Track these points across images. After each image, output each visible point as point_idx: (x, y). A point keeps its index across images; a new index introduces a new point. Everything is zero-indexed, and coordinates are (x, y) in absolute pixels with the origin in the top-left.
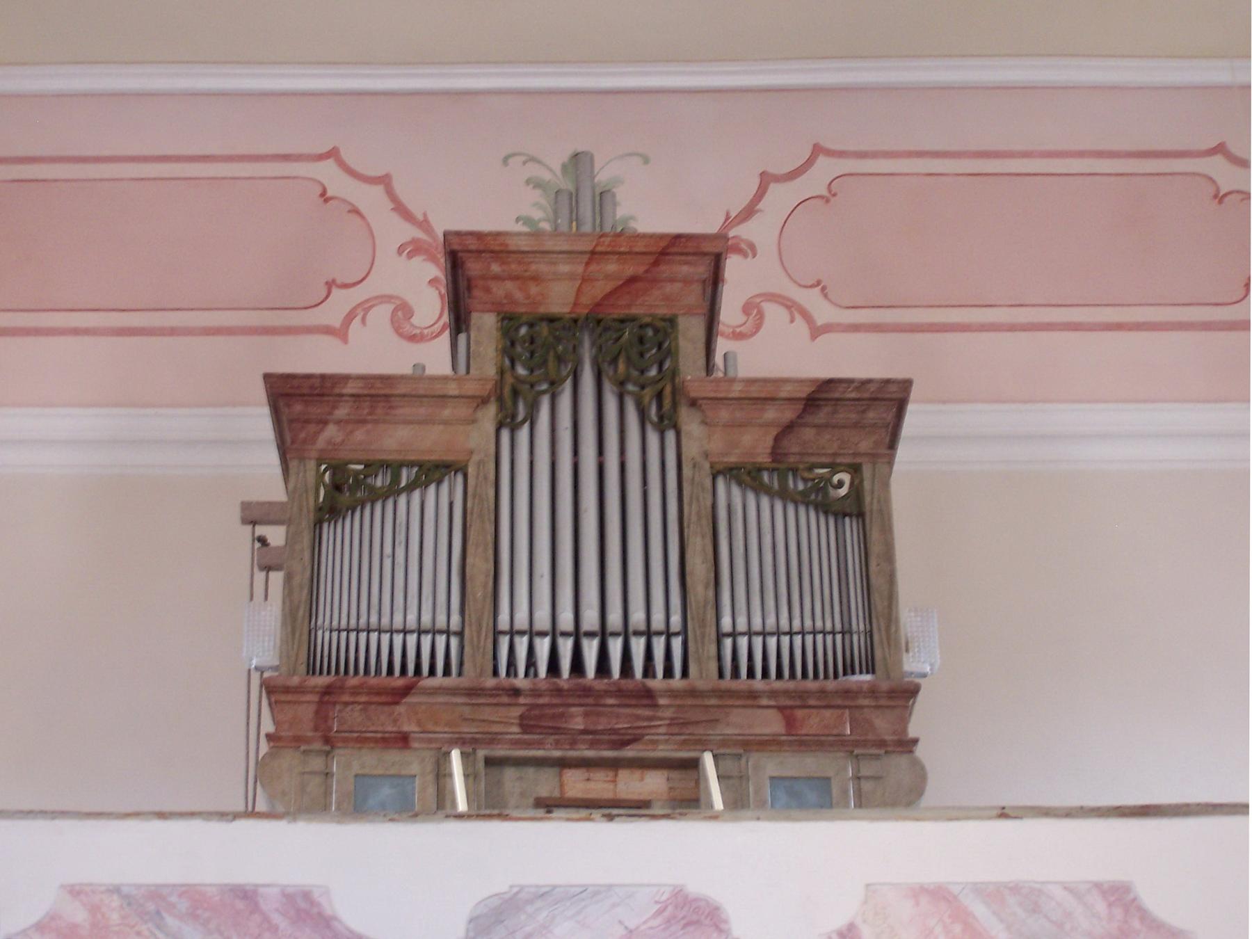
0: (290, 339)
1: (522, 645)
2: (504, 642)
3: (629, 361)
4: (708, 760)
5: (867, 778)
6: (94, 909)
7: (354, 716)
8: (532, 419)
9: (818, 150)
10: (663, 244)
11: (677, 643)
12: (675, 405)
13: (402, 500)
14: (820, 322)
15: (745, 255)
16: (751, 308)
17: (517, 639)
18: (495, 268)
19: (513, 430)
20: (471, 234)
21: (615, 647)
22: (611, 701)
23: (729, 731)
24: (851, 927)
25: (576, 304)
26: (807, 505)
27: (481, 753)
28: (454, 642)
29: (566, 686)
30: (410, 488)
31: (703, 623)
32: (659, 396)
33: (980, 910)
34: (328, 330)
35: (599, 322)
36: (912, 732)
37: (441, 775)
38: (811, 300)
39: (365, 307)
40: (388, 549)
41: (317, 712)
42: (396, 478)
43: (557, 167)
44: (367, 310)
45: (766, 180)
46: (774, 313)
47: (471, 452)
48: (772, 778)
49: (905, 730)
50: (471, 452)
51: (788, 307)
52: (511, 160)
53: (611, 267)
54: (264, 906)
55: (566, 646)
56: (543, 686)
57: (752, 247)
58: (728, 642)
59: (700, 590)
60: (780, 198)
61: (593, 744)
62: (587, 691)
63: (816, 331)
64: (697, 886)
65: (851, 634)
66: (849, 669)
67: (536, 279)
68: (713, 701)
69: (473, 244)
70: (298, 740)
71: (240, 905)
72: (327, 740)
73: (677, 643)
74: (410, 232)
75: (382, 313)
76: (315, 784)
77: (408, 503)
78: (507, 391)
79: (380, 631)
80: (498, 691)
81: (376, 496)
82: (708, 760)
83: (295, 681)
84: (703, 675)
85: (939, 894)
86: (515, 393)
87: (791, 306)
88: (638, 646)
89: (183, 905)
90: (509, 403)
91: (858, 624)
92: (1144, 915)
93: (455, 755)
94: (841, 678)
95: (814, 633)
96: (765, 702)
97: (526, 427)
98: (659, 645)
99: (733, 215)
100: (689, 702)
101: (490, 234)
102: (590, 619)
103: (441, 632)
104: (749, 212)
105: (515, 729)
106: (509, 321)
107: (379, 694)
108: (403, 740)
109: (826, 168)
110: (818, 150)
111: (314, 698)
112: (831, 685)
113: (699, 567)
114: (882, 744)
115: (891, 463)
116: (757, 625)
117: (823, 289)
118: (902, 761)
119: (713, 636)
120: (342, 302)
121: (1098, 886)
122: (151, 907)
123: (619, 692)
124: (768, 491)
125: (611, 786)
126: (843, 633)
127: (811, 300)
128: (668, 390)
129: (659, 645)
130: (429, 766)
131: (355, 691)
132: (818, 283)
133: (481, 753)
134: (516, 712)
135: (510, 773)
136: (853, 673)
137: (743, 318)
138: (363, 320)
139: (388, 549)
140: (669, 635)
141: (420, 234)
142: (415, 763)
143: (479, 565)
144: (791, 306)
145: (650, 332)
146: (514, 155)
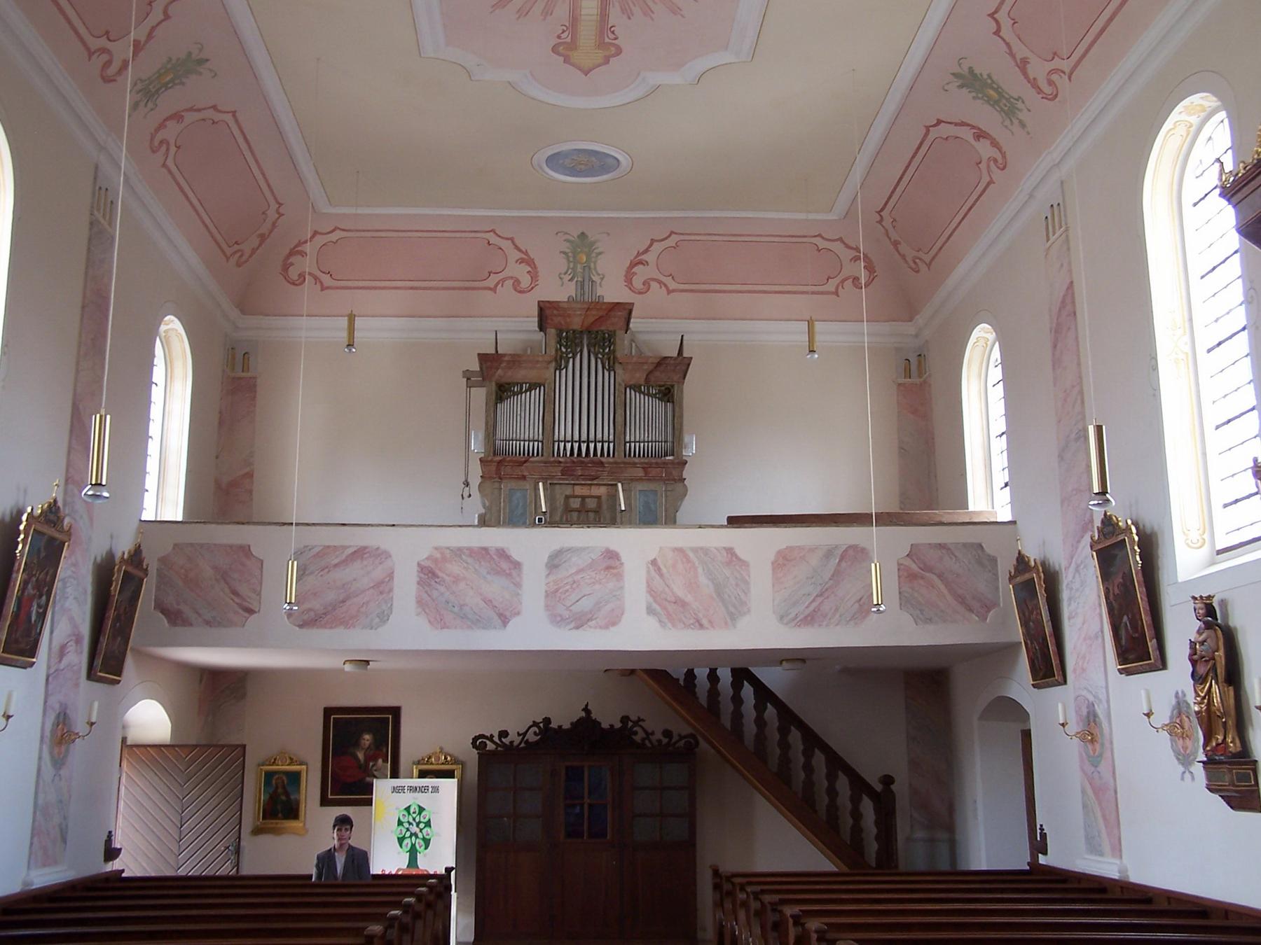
0: (475, 292)
1: (562, 445)
2: (556, 444)
3: (599, 345)
4: (620, 485)
5: (669, 491)
6: (442, 554)
7: (508, 470)
8: (566, 367)
9: (672, 233)
10: (612, 306)
11: (611, 445)
12: (614, 363)
13: (524, 395)
14: (671, 288)
15: (644, 265)
16: (646, 283)
17: (560, 443)
18: (555, 312)
19: (561, 370)
20: (548, 302)
21: (592, 446)
22: (590, 465)
23: (626, 475)
24: (655, 559)
25: (582, 326)
26: (656, 398)
27: (549, 482)
28: (540, 444)
29: (575, 460)
30: (526, 391)
31: (620, 439)
32: (609, 359)
33: (691, 555)
34: (490, 289)
35: (589, 332)
36: (684, 477)
37: (536, 489)
38: (668, 281)
39: (503, 280)
40: (519, 413)
41: (497, 468)
42: (521, 388)
43: (576, 237)
44: (503, 282)
45: (653, 241)
46: (654, 285)
47: (546, 380)
48: (640, 491)
49: (682, 476)
50: (546, 380)
51: (660, 283)
52: (559, 234)
53: (594, 312)
54: (491, 553)
55: (576, 445)
56: (569, 460)
57: (647, 262)
58: (628, 445)
59: (619, 427)
60: (657, 247)
61: (583, 480)
62: (583, 462)
63: (669, 292)
64: (612, 548)
65: (667, 442)
66: (666, 455)
67: (569, 316)
68: (622, 465)
69: (548, 305)
70: (491, 478)
71: (484, 552)
72: (501, 479)
73: (611, 445)
74: (519, 255)
75: (509, 283)
76: (496, 492)
77: (525, 396)
78: (558, 357)
79: (516, 440)
80: (555, 462)
81: (515, 394)
82: (620, 485)
83: (490, 458)
84: (620, 456)
85: (680, 551)
86: (561, 358)
87: (660, 282)
88: (599, 445)
89: (467, 552)
90: (559, 361)
91: (670, 438)
92: (737, 557)
93: (541, 484)
94: (663, 458)
95: (655, 442)
96: (638, 466)
97: (564, 370)
98: (606, 445)
99: (641, 252)
100: (615, 465)
101: (553, 302)
102: (584, 437)
103: (536, 441)
104: (646, 251)
105: (560, 474)
106: (560, 332)
107: (517, 462)
108: (524, 478)
109: (674, 238)
110: (672, 233)
111: (496, 464)
112: (659, 461)
113: (620, 419)
114: (674, 480)
115: (683, 383)
116: (637, 440)
117: (673, 277)
118: (680, 485)
119: (623, 442)
120: (493, 279)
121: (724, 548)
122: (458, 553)
123: (593, 462)
124: (640, 392)
125: (588, 491)
126: (665, 442)
127: (668, 281)
128: (612, 357)
129: (606, 445)
130: (533, 486)
131: (509, 461)
132: (671, 275)
133: (549, 482)
134: (561, 468)
135: (557, 487)
136: (667, 456)
137: (642, 286)
138: (502, 285)
139: (519, 413)
140: (609, 442)
141: (524, 256)
142: (527, 485)
143: (548, 418)
144: (660, 282)
145: (607, 335)
146: (560, 232)
